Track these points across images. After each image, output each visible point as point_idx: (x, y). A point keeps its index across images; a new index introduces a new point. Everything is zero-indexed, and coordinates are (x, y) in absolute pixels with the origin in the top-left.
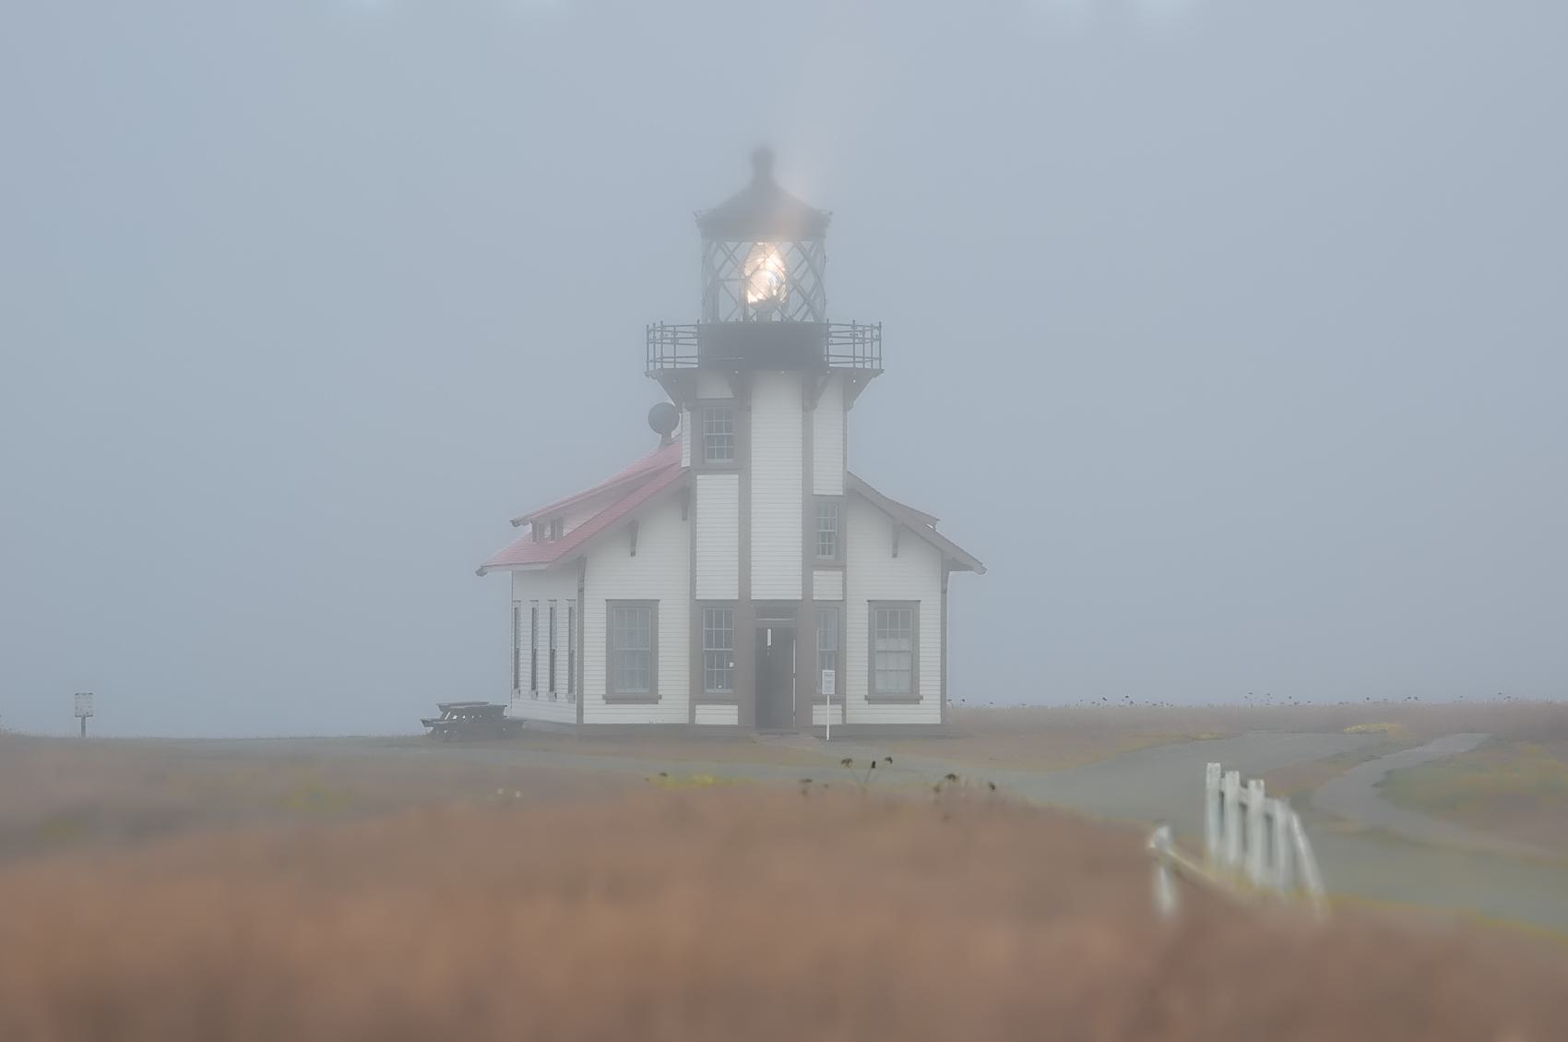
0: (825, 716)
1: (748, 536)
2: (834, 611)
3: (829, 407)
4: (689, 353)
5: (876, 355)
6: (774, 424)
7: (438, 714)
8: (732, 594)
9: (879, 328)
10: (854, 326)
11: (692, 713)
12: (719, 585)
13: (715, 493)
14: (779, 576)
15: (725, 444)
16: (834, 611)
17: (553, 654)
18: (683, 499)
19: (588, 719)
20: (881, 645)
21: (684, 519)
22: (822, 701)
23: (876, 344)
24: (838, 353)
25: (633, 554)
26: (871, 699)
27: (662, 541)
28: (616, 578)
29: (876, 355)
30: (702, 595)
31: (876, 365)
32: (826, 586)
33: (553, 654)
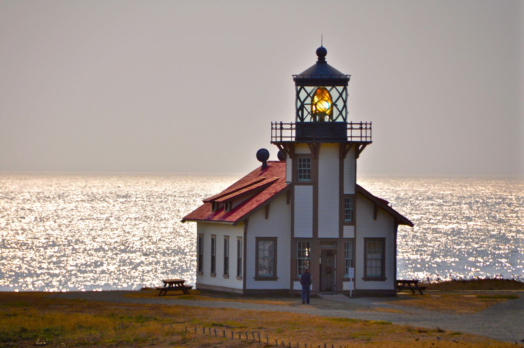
0: (347, 286)
1: (316, 214)
2: (353, 240)
3: (349, 155)
4: (289, 135)
5: (274, 131)
6: (327, 161)
7: (162, 285)
8: (311, 236)
9: (371, 124)
10: (281, 124)
11: (292, 285)
12: (304, 231)
13: (303, 193)
14: (329, 230)
15: (305, 172)
16: (353, 240)
17: (226, 260)
18: (288, 193)
19: (248, 287)
20: (369, 256)
21: (288, 203)
22: (348, 280)
23: (369, 131)
24: (353, 135)
25: (267, 218)
26: (366, 278)
27: (279, 211)
28: (261, 227)
29: (274, 131)
30: (296, 235)
31: (368, 140)
32: (348, 232)
33: (226, 260)
